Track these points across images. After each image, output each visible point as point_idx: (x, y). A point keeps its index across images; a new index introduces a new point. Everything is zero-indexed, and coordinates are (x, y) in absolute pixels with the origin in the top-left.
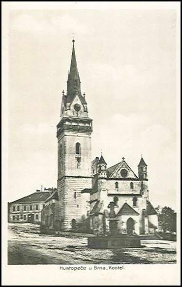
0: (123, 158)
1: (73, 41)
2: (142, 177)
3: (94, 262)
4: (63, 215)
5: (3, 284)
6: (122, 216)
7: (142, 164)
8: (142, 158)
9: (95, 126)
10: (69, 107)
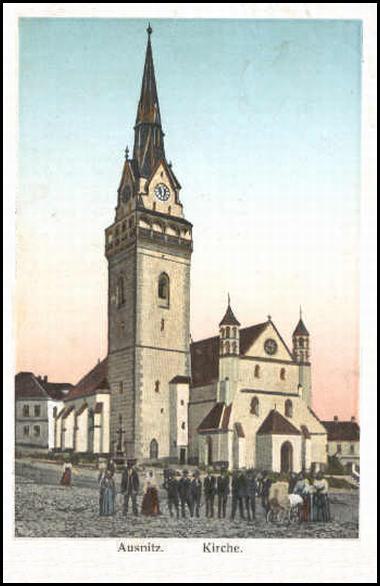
0: (269, 317)
1: (150, 31)
2: (300, 358)
3: (337, 533)
4: (80, 464)
5: (6, 580)
6: (274, 436)
7: (301, 331)
8: (301, 322)
9: (197, 237)
10: (147, 189)
